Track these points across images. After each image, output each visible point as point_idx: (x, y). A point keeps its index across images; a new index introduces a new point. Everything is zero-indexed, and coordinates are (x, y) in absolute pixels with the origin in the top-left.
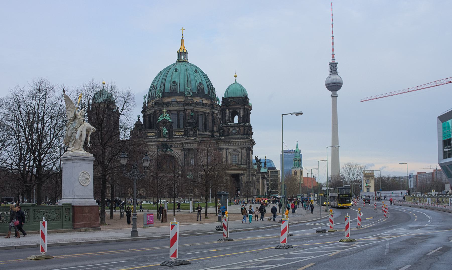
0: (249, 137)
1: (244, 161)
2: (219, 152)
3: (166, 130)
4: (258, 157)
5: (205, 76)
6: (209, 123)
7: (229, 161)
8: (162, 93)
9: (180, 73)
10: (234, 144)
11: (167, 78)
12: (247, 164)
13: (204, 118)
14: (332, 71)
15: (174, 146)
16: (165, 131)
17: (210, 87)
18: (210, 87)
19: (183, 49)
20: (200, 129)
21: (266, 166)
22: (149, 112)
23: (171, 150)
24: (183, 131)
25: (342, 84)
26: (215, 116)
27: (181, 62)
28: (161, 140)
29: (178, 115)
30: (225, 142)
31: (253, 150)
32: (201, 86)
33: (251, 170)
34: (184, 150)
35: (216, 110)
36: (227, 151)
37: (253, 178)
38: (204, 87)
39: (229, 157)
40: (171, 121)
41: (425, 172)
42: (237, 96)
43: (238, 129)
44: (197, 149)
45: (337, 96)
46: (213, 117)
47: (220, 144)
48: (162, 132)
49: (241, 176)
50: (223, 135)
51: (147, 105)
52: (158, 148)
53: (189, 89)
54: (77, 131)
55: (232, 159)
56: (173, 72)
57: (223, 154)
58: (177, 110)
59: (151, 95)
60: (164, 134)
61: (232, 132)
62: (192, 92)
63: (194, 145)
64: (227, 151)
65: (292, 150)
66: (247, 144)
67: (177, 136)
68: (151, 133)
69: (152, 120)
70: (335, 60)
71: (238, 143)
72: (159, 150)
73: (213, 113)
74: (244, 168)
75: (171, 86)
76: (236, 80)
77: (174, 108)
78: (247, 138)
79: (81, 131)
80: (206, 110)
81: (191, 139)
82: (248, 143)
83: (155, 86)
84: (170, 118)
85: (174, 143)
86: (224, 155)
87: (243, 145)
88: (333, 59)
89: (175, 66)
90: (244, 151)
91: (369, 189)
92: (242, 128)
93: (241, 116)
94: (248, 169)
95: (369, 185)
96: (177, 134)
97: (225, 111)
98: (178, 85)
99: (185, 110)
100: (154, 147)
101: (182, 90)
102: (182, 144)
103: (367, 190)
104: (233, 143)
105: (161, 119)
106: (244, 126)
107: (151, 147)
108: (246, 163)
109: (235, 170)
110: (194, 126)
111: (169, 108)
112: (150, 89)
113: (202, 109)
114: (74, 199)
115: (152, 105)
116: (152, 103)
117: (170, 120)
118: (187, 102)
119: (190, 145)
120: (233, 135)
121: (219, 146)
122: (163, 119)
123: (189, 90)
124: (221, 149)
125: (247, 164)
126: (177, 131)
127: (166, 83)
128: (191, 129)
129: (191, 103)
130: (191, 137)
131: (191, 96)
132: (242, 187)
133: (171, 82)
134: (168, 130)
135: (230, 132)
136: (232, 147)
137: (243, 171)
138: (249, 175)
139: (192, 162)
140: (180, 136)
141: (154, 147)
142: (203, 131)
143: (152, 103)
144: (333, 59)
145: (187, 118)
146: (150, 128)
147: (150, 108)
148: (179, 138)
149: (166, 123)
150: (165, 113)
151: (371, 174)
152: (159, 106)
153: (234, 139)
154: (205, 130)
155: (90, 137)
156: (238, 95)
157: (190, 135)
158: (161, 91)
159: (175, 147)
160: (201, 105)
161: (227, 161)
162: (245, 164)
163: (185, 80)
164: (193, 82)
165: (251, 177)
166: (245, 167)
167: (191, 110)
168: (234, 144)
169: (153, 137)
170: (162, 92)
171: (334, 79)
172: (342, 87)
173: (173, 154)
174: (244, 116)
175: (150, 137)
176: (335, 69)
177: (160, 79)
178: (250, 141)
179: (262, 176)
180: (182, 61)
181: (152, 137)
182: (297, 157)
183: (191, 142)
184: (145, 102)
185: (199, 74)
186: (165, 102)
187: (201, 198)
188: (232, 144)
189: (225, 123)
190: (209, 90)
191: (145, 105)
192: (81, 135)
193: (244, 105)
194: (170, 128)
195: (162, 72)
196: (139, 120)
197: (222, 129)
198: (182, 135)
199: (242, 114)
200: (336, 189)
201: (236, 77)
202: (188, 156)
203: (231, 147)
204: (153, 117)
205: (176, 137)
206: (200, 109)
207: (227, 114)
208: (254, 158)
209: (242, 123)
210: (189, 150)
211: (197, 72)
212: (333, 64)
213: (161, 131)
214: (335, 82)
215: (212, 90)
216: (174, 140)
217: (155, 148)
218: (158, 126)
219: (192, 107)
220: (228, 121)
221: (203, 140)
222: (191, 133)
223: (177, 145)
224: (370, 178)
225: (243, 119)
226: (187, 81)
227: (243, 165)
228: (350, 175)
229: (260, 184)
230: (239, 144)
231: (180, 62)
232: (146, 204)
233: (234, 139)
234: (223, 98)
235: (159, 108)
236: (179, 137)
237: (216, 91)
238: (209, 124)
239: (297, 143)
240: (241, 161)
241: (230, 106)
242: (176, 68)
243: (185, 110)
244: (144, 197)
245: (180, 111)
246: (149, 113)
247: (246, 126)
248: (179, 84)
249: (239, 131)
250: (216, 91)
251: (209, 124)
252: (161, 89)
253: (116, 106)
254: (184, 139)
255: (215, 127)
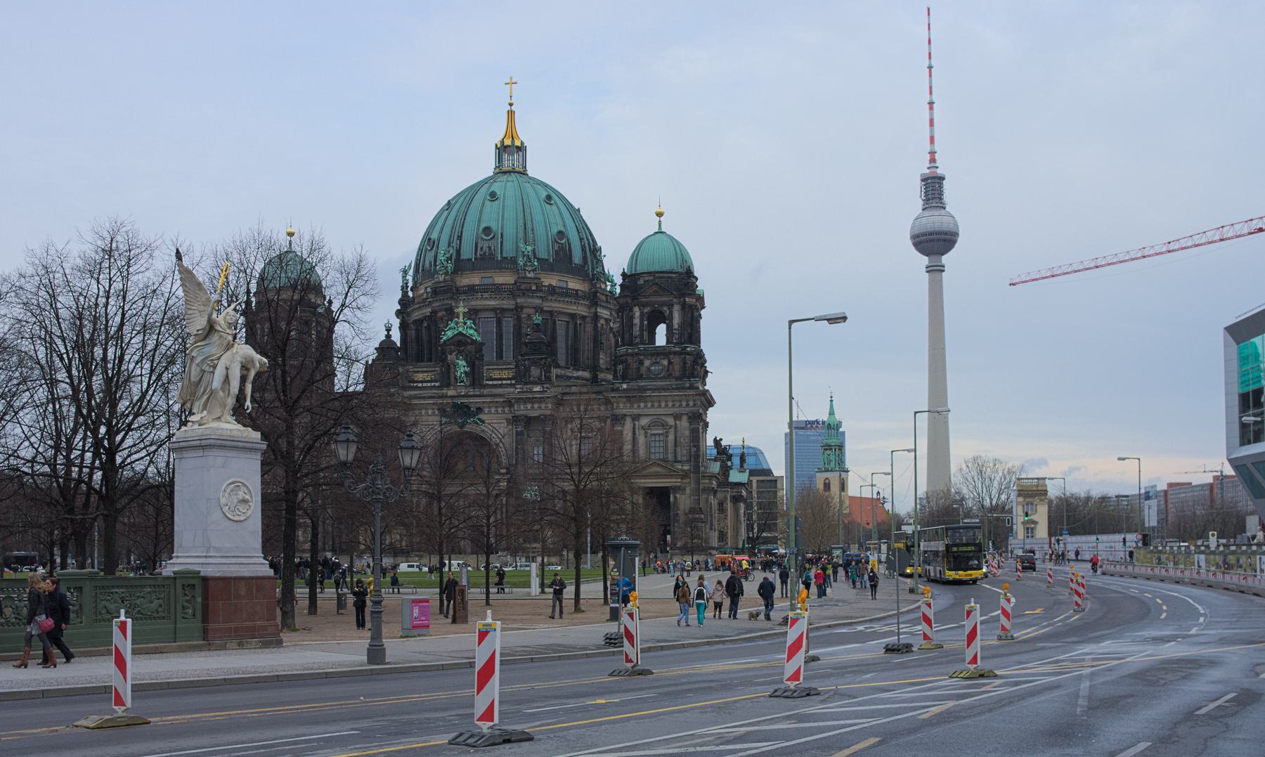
0: (696, 385)
1: (682, 453)
2: (613, 425)
3: (465, 364)
4: (721, 440)
5: (575, 213)
6: (586, 346)
7: (642, 452)
8: (453, 260)
9: (504, 206)
10: (656, 405)
11: (468, 219)
12: (690, 461)
13: (570, 330)
14: (928, 200)
15: (486, 410)
16: (462, 366)
17: (587, 245)
18: (587, 245)
19: (513, 138)
20: (559, 362)
21: (745, 466)
22: (416, 315)
23: (479, 419)
24: (513, 367)
25: (958, 234)
26: (602, 325)
27: (505, 173)
28: (451, 392)
29: (499, 322)
30: (631, 398)
31: (708, 420)
32: (563, 241)
33: (704, 477)
34: (515, 420)
35: (605, 308)
36: (634, 425)
37: (707, 499)
38: (570, 245)
39: (641, 440)
40: (479, 339)
41: (1191, 484)
42: (664, 269)
43: (665, 362)
44: (552, 419)
45: (942, 268)
46: (596, 327)
47: (615, 405)
48: (452, 370)
49: (675, 493)
50: (624, 378)
51: (410, 294)
52: (442, 416)
53: (529, 248)
54: (215, 367)
55: (648, 447)
56: (483, 203)
57: (625, 432)
58: (494, 310)
59: (423, 267)
60: (460, 376)
61: (648, 369)
62: (538, 259)
63: (543, 406)
64: (637, 423)
65: (817, 421)
66: (691, 403)
67: (495, 382)
68: (423, 372)
69: (424, 337)
70: (937, 167)
71: (666, 402)
72: (444, 420)
73: (596, 317)
74: (683, 471)
75: (480, 241)
76: (660, 225)
77: (488, 303)
78: (692, 387)
79: (227, 369)
80: (575, 308)
81: (535, 390)
82: (694, 401)
83: (434, 242)
84: (475, 330)
85: (488, 400)
86: (628, 436)
87: (680, 406)
88: (932, 165)
89: (490, 186)
90: (684, 423)
91: (1032, 529)
92: (676, 360)
93: (676, 326)
94: (694, 473)
95: (1034, 517)
96: (496, 375)
97: (631, 310)
98: (498, 238)
99: (518, 309)
100: (430, 412)
101: (509, 251)
102: (509, 403)
103: (1028, 533)
104: (652, 402)
105: (450, 334)
106: (683, 354)
107: (423, 412)
108: (688, 457)
109: (657, 476)
110: (542, 354)
111: (473, 303)
112: (419, 249)
113: (565, 306)
114: (206, 557)
115: (425, 295)
116: (426, 288)
117: (476, 337)
118: (523, 287)
119: (533, 407)
120: (653, 378)
121: (613, 409)
122: (456, 332)
123: (530, 254)
124: (618, 419)
125: (692, 459)
126: (496, 367)
127: (463, 234)
128: (535, 363)
129: (534, 288)
130: (536, 383)
131: (534, 270)
132: (676, 524)
133: (478, 229)
134: (471, 364)
135: (643, 370)
136: (648, 411)
137: (679, 480)
138: (697, 492)
139: (537, 453)
140: (504, 382)
141: (430, 412)
142: (568, 368)
143: (426, 288)
144: (932, 165)
145: (524, 331)
146: (419, 358)
147: (419, 303)
148: (501, 386)
149: (466, 344)
150: (461, 317)
151: (1040, 488)
152: (446, 296)
153: (656, 389)
154: (574, 365)
155: (251, 385)
156: (667, 267)
157: (532, 379)
158: (451, 255)
159: (490, 413)
160: (562, 296)
161: (634, 450)
162: (684, 459)
163: (517, 225)
164: (540, 230)
165: (703, 497)
166: (686, 468)
167: (535, 308)
168: (656, 405)
169: (429, 384)
170: (454, 257)
171: (935, 221)
172: (956, 245)
173: (483, 431)
174: (682, 325)
175: (420, 385)
176: (936, 192)
177: (447, 222)
178: (699, 395)
179: (735, 494)
180: (510, 172)
181: (425, 385)
182: (831, 441)
183: (536, 398)
184: (407, 287)
185: (558, 207)
186: (462, 285)
187: (562, 555)
188: (649, 405)
189: (631, 344)
190: (585, 253)
191: (405, 294)
192: (227, 379)
193: (683, 295)
194: (477, 358)
195: (453, 202)
196: (388, 336)
197: (622, 362)
198: (508, 379)
199: (676, 321)
200: (939, 531)
201: (660, 215)
202: (526, 436)
203: (646, 411)
204: (428, 328)
205: (493, 385)
206: (559, 305)
207: (637, 321)
208: (710, 442)
209: (676, 344)
210: (529, 421)
211: (553, 202)
212: (933, 181)
213: (452, 366)
214: (937, 229)
215: (592, 251)
216: (486, 391)
217: (434, 414)
218: (443, 352)
219: (538, 301)
220: (638, 340)
221: (569, 394)
222: (535, 372)
223: (497, 407)
224: (1036, 500)
225: (681, 334)
226: (523, 227)
227: (680, 462)
228: (980, 492)
229: (727, 515)
230: (670, 404)
231: (503, 173)
232: (408, 573)
233: (656, 389)
234: (624, 275)
235: (445, 302)
236: (502, 384)
237: (605, 256)
238: (586, 348)
239: (831, 401)
240: (675, 451)
241: (645, 297)
242: (492, 189)
243: (518, 309)
244: (404, 553)
245: (503, 310)
246: (416, 318)
247: (688, 354)
248: (502, 237)
249: (668, 367)
250: (605, 256)
251: (586, 348)
252: (451, 248)
253: (324, 297)
254: (516, 389)
255: (601, 356)
